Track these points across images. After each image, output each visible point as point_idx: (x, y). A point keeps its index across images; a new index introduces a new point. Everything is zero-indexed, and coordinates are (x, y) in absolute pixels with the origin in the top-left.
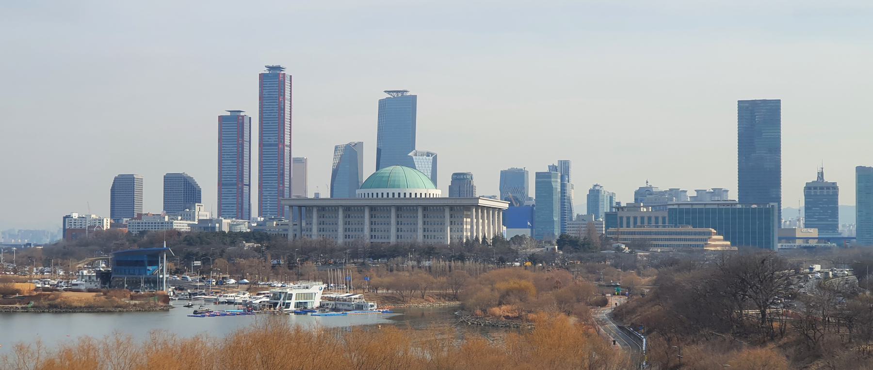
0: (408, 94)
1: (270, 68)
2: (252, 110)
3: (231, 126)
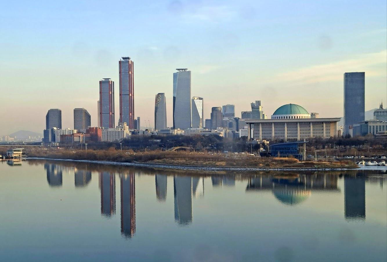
0: (187, 70)
1: (124, 58)
2: (115, 79)
3: (105, 86)
